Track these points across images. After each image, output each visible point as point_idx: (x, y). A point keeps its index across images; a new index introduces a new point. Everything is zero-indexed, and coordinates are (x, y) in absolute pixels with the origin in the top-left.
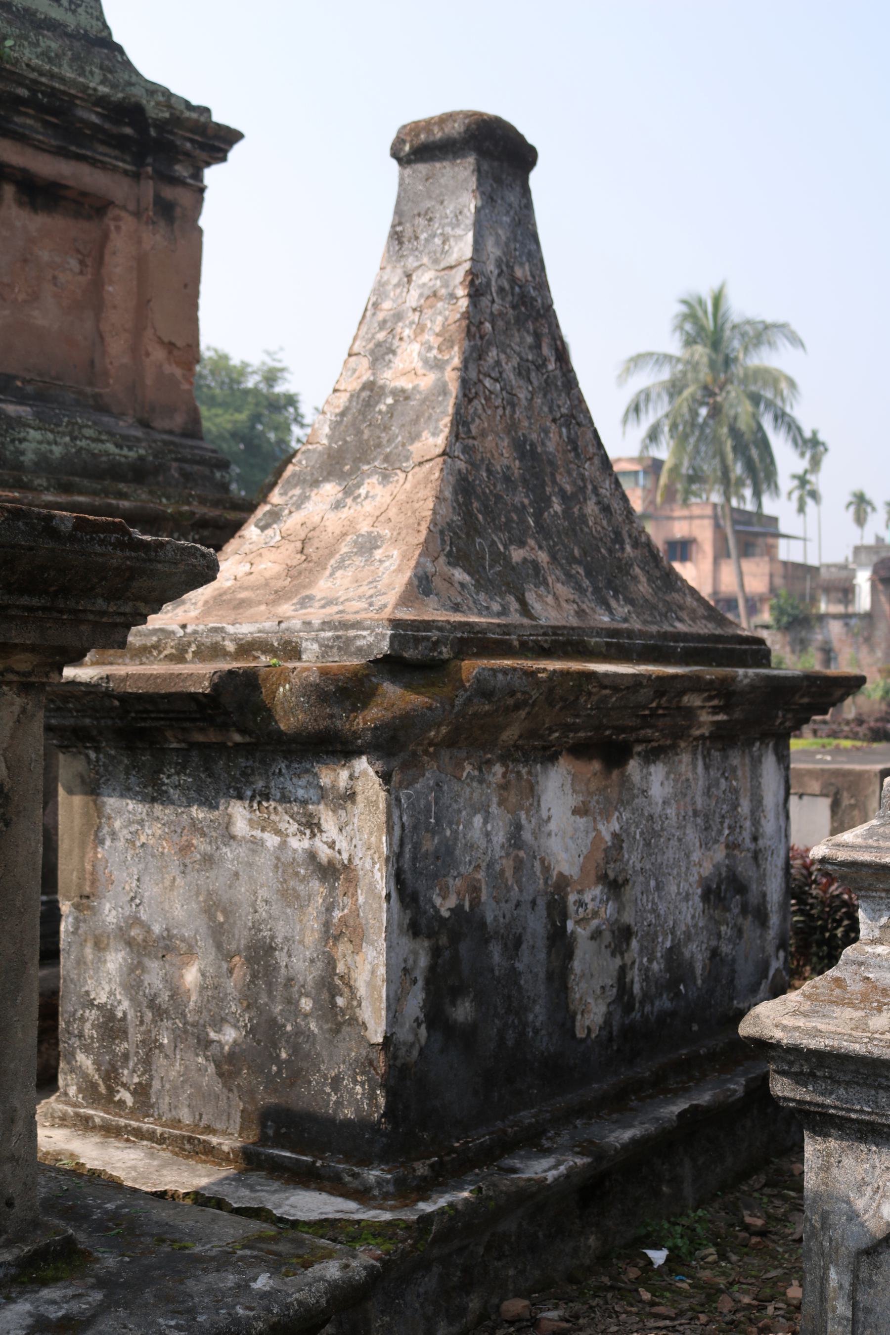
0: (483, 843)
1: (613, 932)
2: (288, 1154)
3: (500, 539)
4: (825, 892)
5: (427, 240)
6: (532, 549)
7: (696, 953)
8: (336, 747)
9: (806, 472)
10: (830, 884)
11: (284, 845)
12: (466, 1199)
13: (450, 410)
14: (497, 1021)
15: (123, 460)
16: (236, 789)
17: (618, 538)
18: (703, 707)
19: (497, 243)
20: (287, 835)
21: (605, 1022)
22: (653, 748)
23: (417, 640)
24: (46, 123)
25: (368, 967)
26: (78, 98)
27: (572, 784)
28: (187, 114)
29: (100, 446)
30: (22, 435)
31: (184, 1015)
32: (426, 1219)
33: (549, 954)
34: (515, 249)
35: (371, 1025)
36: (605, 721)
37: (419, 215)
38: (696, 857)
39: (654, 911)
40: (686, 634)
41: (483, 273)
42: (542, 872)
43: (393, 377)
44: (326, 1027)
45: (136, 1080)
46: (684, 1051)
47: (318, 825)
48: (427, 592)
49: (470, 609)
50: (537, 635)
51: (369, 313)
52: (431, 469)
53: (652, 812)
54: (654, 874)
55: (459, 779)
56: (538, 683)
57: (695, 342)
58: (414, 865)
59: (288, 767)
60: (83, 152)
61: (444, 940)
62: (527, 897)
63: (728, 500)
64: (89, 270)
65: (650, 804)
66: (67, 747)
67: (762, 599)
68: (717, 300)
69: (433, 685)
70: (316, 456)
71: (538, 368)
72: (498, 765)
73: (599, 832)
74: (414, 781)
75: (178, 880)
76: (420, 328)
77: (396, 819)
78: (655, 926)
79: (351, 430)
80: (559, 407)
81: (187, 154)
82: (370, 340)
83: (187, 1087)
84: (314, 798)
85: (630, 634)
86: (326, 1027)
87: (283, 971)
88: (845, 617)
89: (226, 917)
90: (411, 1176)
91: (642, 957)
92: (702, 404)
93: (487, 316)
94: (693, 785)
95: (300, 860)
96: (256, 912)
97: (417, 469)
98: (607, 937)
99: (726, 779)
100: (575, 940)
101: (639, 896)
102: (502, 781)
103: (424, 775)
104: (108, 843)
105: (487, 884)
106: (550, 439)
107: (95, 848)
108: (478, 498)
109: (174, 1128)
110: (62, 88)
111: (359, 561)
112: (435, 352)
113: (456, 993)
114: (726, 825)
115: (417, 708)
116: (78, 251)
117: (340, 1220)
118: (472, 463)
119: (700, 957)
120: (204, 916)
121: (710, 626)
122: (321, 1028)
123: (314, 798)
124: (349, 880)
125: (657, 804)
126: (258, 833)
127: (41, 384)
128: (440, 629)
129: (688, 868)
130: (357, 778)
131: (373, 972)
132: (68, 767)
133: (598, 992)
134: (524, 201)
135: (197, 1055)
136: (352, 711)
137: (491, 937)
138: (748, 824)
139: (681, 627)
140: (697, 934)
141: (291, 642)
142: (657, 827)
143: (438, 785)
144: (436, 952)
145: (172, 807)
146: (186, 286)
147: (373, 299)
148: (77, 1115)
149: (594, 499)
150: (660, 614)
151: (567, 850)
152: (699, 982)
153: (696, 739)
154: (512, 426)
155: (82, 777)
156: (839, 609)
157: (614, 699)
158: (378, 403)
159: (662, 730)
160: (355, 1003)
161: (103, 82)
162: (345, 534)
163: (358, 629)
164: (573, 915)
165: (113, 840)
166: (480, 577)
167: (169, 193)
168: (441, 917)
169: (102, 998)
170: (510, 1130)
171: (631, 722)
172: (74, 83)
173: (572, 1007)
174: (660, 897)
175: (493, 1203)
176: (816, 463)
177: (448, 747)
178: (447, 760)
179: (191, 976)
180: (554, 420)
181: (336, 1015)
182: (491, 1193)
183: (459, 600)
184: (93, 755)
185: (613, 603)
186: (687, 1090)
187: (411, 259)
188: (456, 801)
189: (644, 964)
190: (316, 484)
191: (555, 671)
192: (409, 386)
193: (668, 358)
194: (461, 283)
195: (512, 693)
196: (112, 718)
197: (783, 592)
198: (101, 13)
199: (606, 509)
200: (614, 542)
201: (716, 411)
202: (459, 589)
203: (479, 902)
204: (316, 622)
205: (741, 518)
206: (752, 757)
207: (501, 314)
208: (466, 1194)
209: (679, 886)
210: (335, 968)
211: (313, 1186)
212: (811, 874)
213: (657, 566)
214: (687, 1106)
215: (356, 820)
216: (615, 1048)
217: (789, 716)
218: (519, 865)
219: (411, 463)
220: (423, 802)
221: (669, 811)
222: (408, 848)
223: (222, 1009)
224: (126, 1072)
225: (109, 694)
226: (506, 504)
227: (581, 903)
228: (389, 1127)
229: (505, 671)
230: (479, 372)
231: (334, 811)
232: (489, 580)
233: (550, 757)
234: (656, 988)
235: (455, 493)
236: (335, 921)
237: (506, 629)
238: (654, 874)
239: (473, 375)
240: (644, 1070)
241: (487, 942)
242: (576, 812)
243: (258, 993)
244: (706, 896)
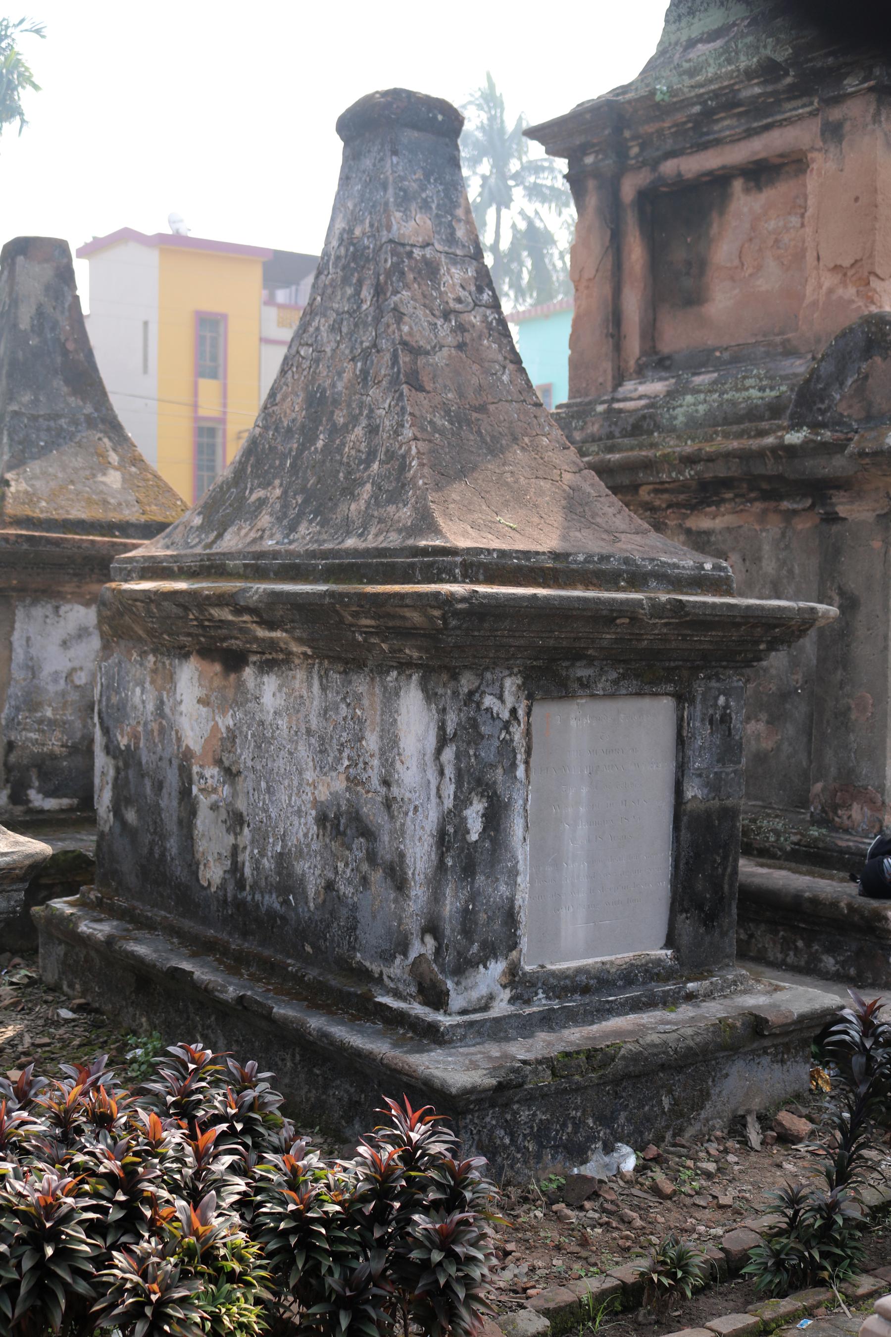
0: (140, 706)
22: (267, 660)
26: (734, 84)
33: (180, 803)
38: (309, 776)
39: (266, 811)
53: (263, 718)
73: (217, 723)
99: (348, 705)
101: (251, 791)
114: (345, 755)
125: (268, 712)
127: (736, 348)
138: (375, 762)
151: (192, 730)
206: (385, 688)
218: (162, 731)
221: (280, 722)
222: (104, 699)
227: (202, 776)
241: (143, 776)
242: (199, 701)
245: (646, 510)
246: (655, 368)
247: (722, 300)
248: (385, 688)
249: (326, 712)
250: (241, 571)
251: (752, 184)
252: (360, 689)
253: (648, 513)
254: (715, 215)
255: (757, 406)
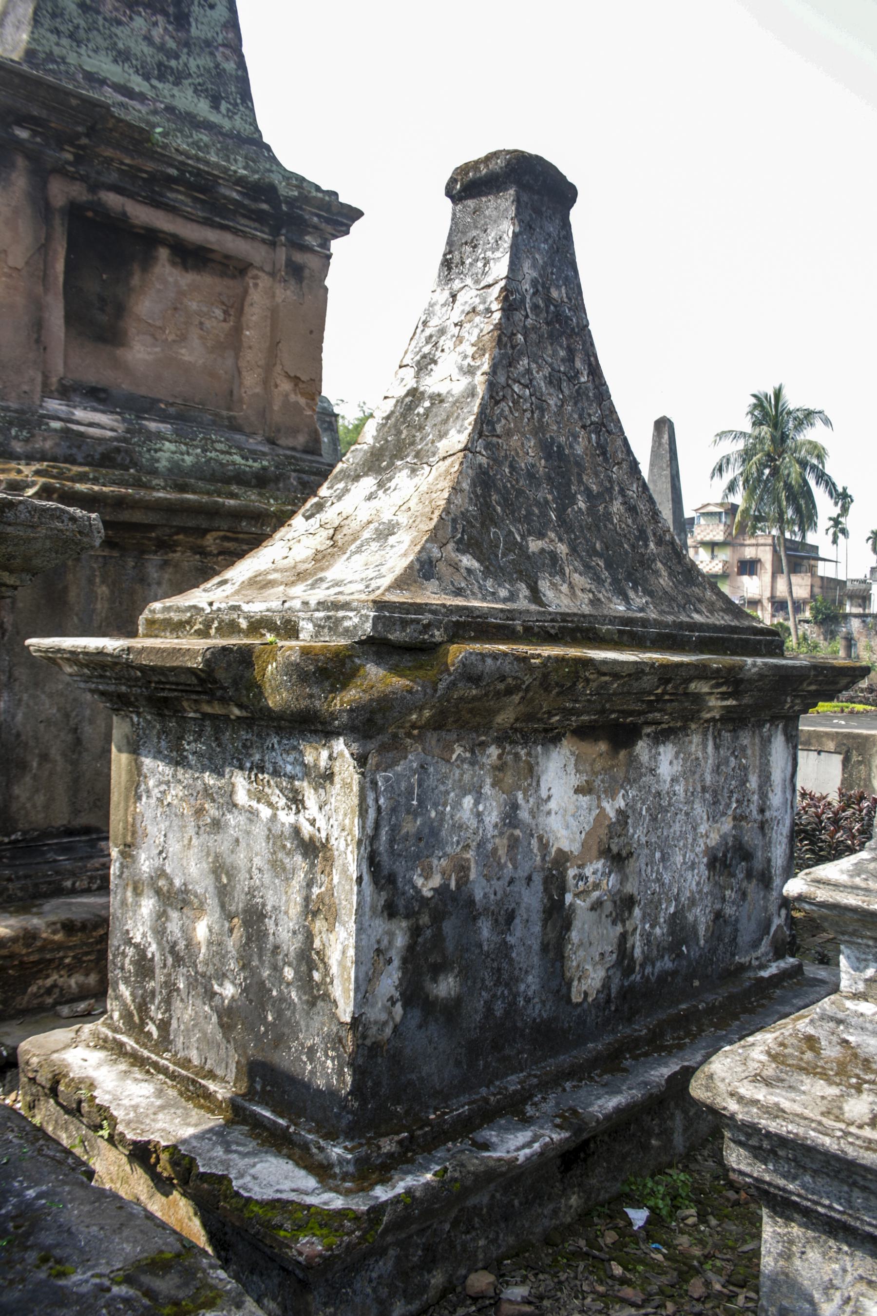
0: (473, 823)
1: (615, 902)
2: (268, 1114)
3: (518, 530)
4: (832, 838)
5: (471, 264)
6: (552, 541)
7: (700, 918)
8: (311, 725)
9: (839, 516)
10: (837, 832)
11: (274, 816)
12: (427, 1184)
13: (476, 410)
14: (483, 993)
15: (247, 469)
16: (239, 760)
17: (642, 535)
18: (711, 694)
19: (534, 266)
20: (277, 809)
21: (603, 986)
22: (663, 730)
23: (404, 623)
24: (196, 200)
25: (340, 947)
27: (576, 765)
28: (314, 193)
29: (228, 457)
30: (158, 446)
31: (195, 966)
32: (377, 1210)
33: (544, 926)
34: (552, 273)
35: (341, 1003)
36: (608, 706)
37: (466, 243)
38: (702, 829)
39: (658, 880)
40: (702, 624)
41: (517, 291)
42: (539, 849)
43: (432, 384)
44: (305, 998)
45: (160, 1016)
46: (684, 1006)
47: (302, 802)
48: (427, 577)
49: (473, 593)
50: (545, 621)
51: (419, 331)
52: (453, 463)
53: (660, 789)
54: (659, 847)
55: (448, 761)
56: (532, 669)
57: (761, 424)
58: (392, 847)
59: (279, 743)
60: (226, 222)
61: (425, 919)
62: (522, 873)
63: (783, 533)
64: (232, 318)
65: (658, 782)
66: (118, 710)
67: (805, 602)
68: (778, 394)
69: (421, 667)
70: (361, 454)
71: (570, 379)
72: (493, 747)
73: (603, 810)
74: (395, 763)
75: (194, 840)
76: (460, 340)
77: (370, 801)
78: (659, 894)
79: (393, 431)
80: (590, 415)
81: (316, 227)
82: (418, 353)
83: (196, 1031)
84: (300, 775)
85: (645, 622)
86: (305, 998)
87: (271, 938)
88: (862, 616)
89: (229, 880)
90: (375, 1154)
91: (645, 923)
92: (766, 466)
93: (520, 329)
94: (702, 763)
95: (287, 833)
96: (251, 878)
97: (441, 463)
98: (609, 907)
99: (736, 757)
100: (574, 911)
101: (644, 867)
102: (499, 763)
103: (406, 758)
104: (144, 799)
105: (476, 862)
106: (578, 443)
107: (135, 803)
108: (498, 491)
109: (183, 1068)
110: (206, 169)
111: (374, 545)
112: (469, 360)
113: (437, 971)
114: (734, 799)
115: (417, 691)
116: (223, 303)
117: (292, 1202)
118: (496, 460)
119: (703, 919)
120: (212, 876)
121: (726, 617)
122: (300, 998)
123: (300, 775)
124: (326, 859)
125: (665, 782)
126: (254, 804)
128: (434, 612)
129: (694, 840)
130: (336, 759)
131: (344, 953)
132: (120, 728)
133: (597, 958)
134: (563, 233)
135: (205, 1004)
136: (331, 692)
137: (480, 914)
138: (756, 797)
139: (697, 617)
140: (701, 899)
141: (291, 621)
142: (665, 803)
143: (422, 767)
144: (415, 932)
145: (190, 771)
146: (311, 332)
147: (423, 318)
148: (115, 1039)
149: (620, 499)
150: (679, 606)
151: (567, 827)
152: (702, 942)
153: (707, 721)
154: (540, 429)
155: (127, 738)
156: (860, 610)
157: (615, 685)
158: (417, 406)
159: (671, 714)
160: (328, 980)
161: (245, 168)
162: (370, 522)
163: (346, 610)
164: (572, 888)
165: (148, 797)
166: (491, 564)
167: (299, 257)
168: (422, 897)
169: (137, 939)
170: (492, 1098)
171: (638, 707)
172: (217, 166)
173: (568, 974)
174: (665, 868)
175: (458, 1185)
176: (845, 510)
177: (435, 729)
178: (434, 742)
179: (201, 931)
180: (584, 427)
181: (313, 988)
182: (457, 1175)
183: (463, 585)
184: (135, 719)
185: (631, 594)
186: (681, 1047)
187: (457, 281)
188: (443, 783)
189: (645, 930)
190: (357, 478)
191: (549, 657)
192: (443, 391)
193: (743, 434)
194: (496, 299)
195: (503, 678)
196: (140, 687)
197: (819, 598)
198: (255, 120)
199: (632, 509)
200: (638, 539)
201: (775, 471)
202: (465, 574)
203: (467, 881)
204: (313, 603)
205: (791, 546)
206: (762, 737)
207: (534, 328)
208: (429, 1176)
209: (684, 856)
210: (312, 943)
211: (285, 1151)
212: (821, 822)
213: (679, 563)
214: (677, 1068)
215: (332, 801)
216: (613, 1008)
217: (798, 701)
218: (514, 844)
219: (436, 458)
220: (403, 785)
221: (677, 788)
223: (223, 964)
224: (153, 1007)
225: (129, 665)
226: (528, 499)
227: (581, 877)
228: (356, 1105)
229: (495, 656)
230: (509, 377)
231: (315, 790)
232: (501, 568)
233: (551, 737)
234: (658, 951)
235: (474, 485)
236: (314, 897)
237: (510, 615)
238: (659, 847)
239: (502, 380)
240: (641, 1028)
241: (475, 919)
242: (578, 791)
243: (251, 956)
244: (711, 865)
245: (195, 553)
246: (85, 395)
247: (140, 352)
248: (762, 737)
249: (718, 767)
250: (616, 637)
251: (178, 260)
252: (745, 742)
253: (198, 557)
254: (136, 267)
255: (244, 472)
